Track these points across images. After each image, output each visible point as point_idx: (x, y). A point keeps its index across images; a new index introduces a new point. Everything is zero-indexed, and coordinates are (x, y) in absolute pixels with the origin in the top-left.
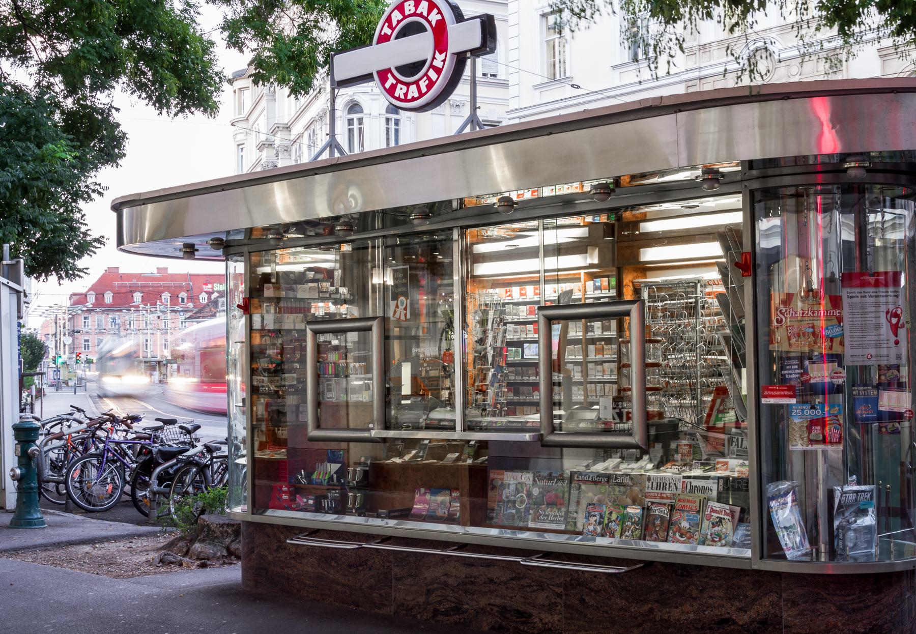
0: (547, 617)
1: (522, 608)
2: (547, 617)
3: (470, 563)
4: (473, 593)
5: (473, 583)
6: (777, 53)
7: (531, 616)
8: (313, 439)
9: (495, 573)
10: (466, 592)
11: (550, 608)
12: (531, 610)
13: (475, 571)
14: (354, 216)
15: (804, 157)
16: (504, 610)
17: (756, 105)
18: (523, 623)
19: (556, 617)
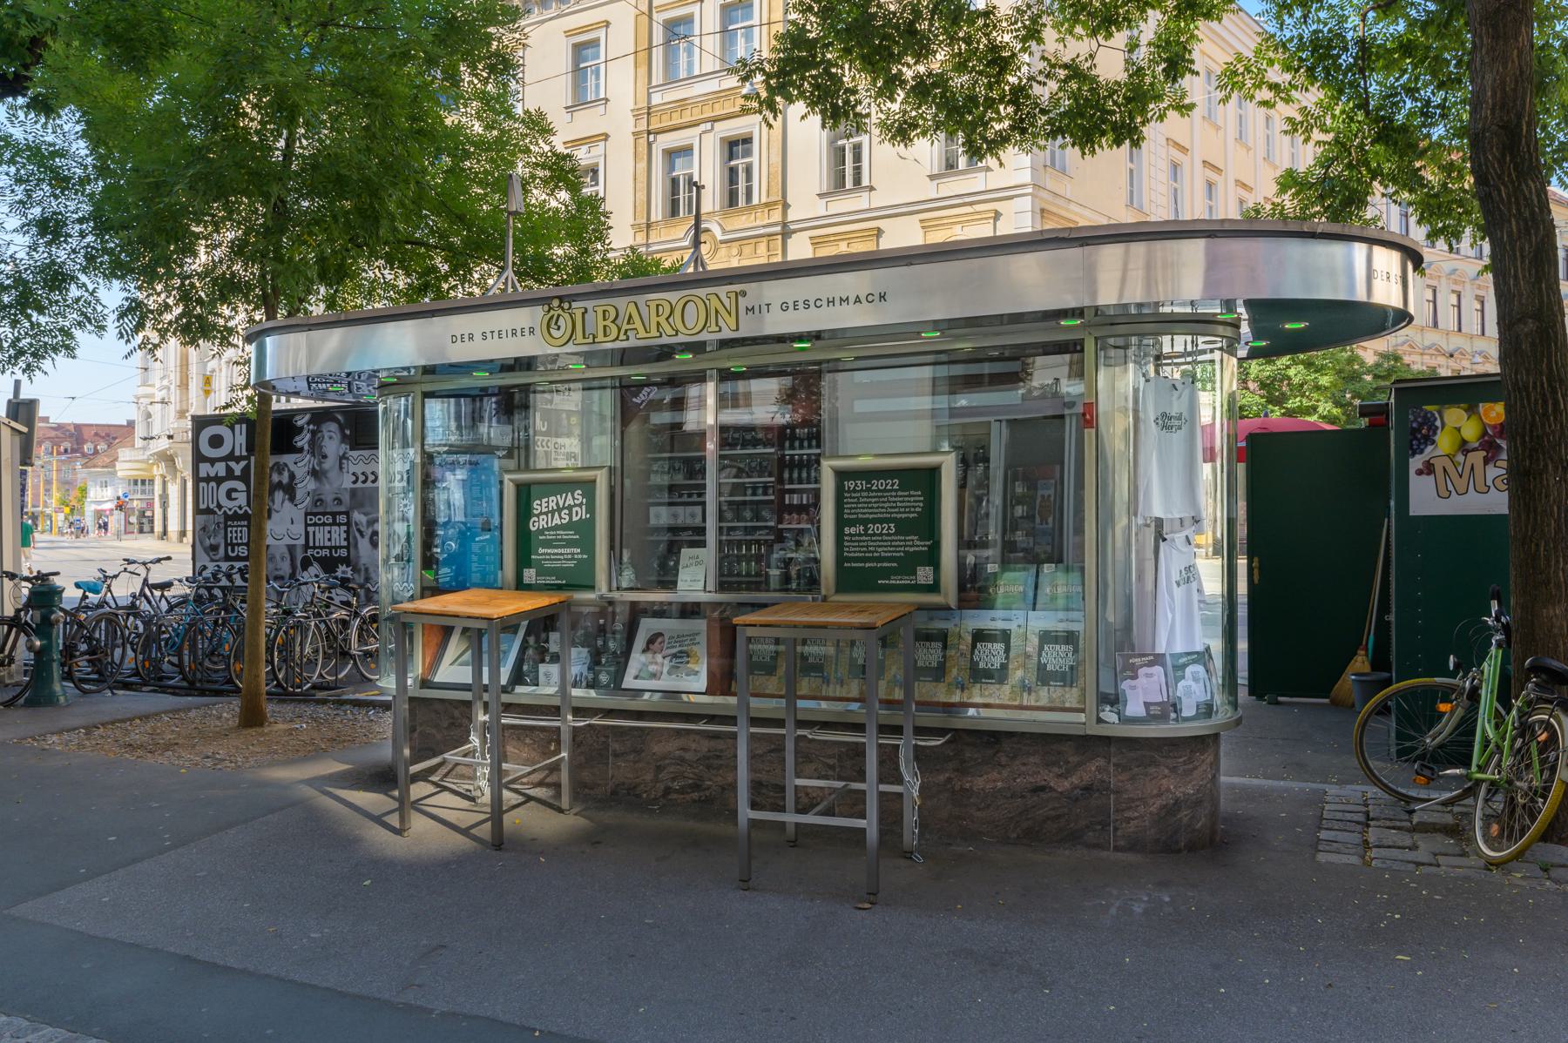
4: (719, 767)
5: (719, 757)
10: (709, 767)
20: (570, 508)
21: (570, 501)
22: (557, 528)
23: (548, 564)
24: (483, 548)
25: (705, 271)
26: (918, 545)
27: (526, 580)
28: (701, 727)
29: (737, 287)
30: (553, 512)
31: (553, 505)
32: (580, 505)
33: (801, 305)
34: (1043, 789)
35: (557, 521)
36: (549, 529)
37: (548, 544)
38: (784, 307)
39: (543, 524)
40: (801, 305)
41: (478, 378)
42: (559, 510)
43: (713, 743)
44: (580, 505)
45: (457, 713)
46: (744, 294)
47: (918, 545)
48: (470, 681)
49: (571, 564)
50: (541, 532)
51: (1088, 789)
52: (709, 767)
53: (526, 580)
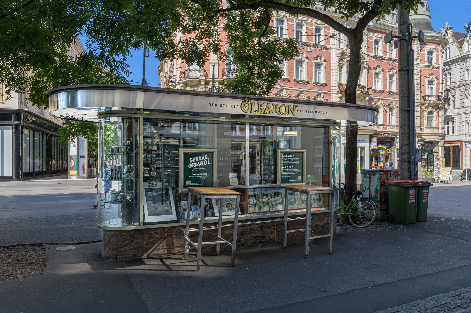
0: (270, 236)
1: (262, 235)
2: (270, 236)
3: (244, 226)
4: (245, 234)
5: (245, 232)
6: (376, 100)
7: (265, 237)
8: (305, 149)
9: (253, 227)
10: (242, 235)
11: (272, 233)
12: (265, 235)
13: (246, 228)
14: (125, 212)
15: (370, 151)
16: (256, 237)
17: (312, 106)
18: (263, 239)
19: (273, 235)
20: (203, 161)
21: (203, 159)
22: (198, 167)
23: (195, 179)
24: (169, 174)
25: (147, 86)
26: (298, 171)
27: (187, 184)
28: (250, 223)
29: (296, 105)
30: (197, 162)
31: (197, 160)
32: (207, 160)
33: (236, 107)
34: (317, 226)
35: (199, 165)
36: (196, 167)
37: (196, 172)
38: (306, 111)
39: (193, 165)
40: (236, 107)
41: (284, 121)
42: (200, 161)
43: (244, 228)
44: (207, 160)
45: (152, 233)
46: (296, 106)
47: (298, 171)
48: (176, 219)
49: (204, 178)
50: (192, 168)
51: (325, 224)
52: (242, 235)
53: (187, 184)
